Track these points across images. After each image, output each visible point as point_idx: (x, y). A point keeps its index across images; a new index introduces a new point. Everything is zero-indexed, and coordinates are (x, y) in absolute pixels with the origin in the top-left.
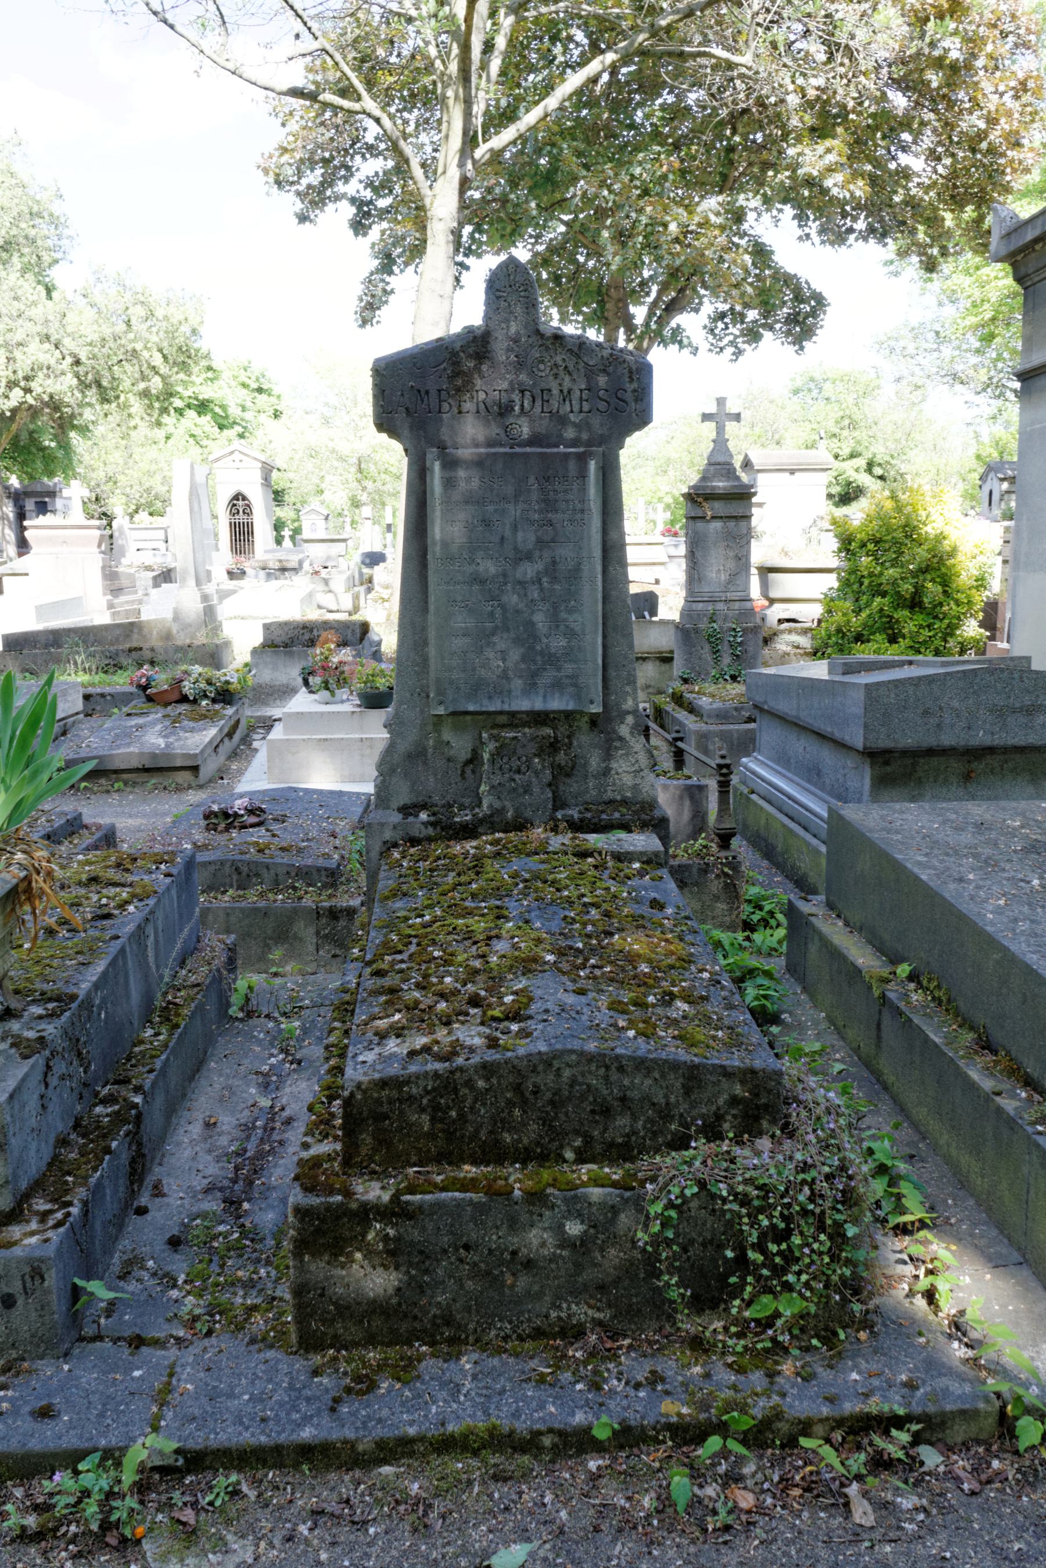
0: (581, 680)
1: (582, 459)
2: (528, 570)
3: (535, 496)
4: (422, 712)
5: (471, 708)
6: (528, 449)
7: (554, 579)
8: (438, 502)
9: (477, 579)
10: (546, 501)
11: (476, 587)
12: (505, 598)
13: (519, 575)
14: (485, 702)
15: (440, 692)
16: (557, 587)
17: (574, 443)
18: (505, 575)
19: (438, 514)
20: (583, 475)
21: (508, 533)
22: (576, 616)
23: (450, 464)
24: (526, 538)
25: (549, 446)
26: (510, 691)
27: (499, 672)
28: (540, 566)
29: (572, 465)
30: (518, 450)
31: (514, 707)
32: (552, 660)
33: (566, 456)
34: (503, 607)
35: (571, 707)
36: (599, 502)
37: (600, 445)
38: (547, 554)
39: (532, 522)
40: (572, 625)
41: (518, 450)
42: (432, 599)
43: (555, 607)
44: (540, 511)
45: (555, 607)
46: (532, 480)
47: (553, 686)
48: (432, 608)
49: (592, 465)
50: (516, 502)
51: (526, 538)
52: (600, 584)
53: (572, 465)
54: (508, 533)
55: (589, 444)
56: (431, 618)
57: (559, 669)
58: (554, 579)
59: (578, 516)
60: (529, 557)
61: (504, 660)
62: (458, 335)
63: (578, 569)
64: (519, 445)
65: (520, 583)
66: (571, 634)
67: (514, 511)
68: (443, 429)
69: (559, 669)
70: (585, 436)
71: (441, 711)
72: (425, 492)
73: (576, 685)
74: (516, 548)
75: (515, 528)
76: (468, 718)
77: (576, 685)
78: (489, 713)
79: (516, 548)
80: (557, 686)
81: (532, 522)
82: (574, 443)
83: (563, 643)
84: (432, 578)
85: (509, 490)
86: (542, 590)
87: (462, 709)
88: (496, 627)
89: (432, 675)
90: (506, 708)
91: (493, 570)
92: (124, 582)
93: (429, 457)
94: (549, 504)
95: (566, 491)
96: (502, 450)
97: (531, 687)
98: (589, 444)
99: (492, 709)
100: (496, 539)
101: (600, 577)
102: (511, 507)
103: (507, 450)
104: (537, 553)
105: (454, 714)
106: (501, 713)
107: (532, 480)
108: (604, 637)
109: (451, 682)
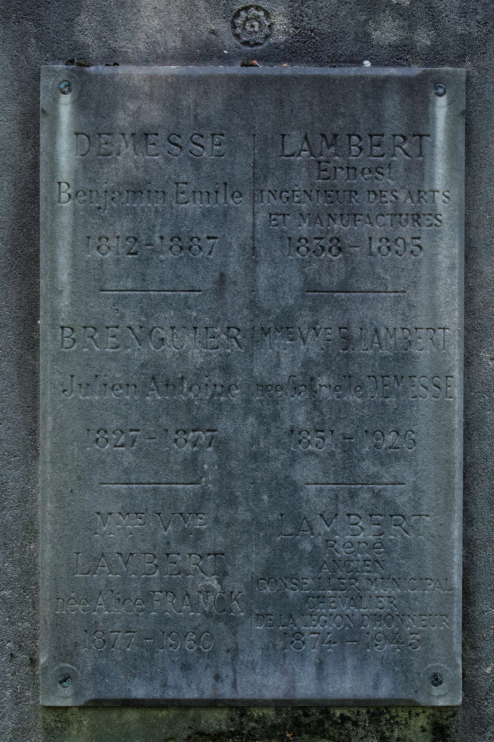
0: (411, 625)
1: (417, 93)
2: (284, 358)
3: (301, 181)
4: (18, 699)
5: (140, 691)
6: (286, 69)
7: (347, 380)
8: (65, 191)
9: (160, 379)
10: (329, 193)
11: (154, 398)
12: (225, 425)
13: (259, 370)
14: (174, 676)
15: (64, 652)
16: (353, 398)
17: (399, 54)
18: (226, 369)
19: (66, 219)
20: (419, 133)
21: (234, 267)
22: (398, 469)
23: (96, 104)
24: (279, 279)
25: (335, 61)
26: (234, 652)
27: (208, 603)
28: (313, 348)
29: (392, 106)
30: (261, 69)
31: (245, 692)
32: (340, 575)
33: (379, 84)
34: (220, 445)
35: (384, 691)
36: (457, 193)
37: (460, 60)
38: (327, 319)
39: (293, 242)
40: (389, 491)
41: (261, 69)
42: (47, 424)
43: (348, 446)
44: (315, 217)
45: (348, 446)
46: (294, 141)
47: (341, 638)
48: (46, 446)
49: (441, 108)
50: (256, 195)
51: (279, 279)
52: (457, 392)
53: (392, 106)
54: (234, 267)
55: (433, 57)
56: (45, 471)
57: (356, 599)
58: (347, 380)
59: (406, 230)
60: (286, 326)
61: (222, 574)
62: (434, 112)
63: (403, 357)
64: (266, 58)
65: (264, 387)
66: (386, 513)
67: (250, 215)
68: (83, 18)
69: (356, 599)
70: (424, 39)
71: (64, 697)
72: (35, 166)
73: (396, 639)
74: (253, 304)
75: (252, 254)
76: (132, 716)
77: (396, 639)
78: (183, 705)
79: (253, 304)
80: (351, 638)
81: (293, 242)
82: (399, 54)
83: (368, 534)
84: (48, 372)
85: (242, 167)
86: (316, 405)
87: (116, 694)
88: (204, 496)
89: (45, 610)
90: (226, 691)
91: (197, 356)
92: (423, 154)
93: (46, 83)
94: (339, 201)
95: (377, 169)
96: (222, 70)
97: (287, 641)
98: (433, 57)
99: (190, 694)
100: (206, 281)
101: (457, 375)
102: (243, 205)
103: (236, 69)
104: (305, 318)
105: (97, 705)
106: (213, 704)
107: (294, 141)
108: (468, 520)
109: (92, 628)
